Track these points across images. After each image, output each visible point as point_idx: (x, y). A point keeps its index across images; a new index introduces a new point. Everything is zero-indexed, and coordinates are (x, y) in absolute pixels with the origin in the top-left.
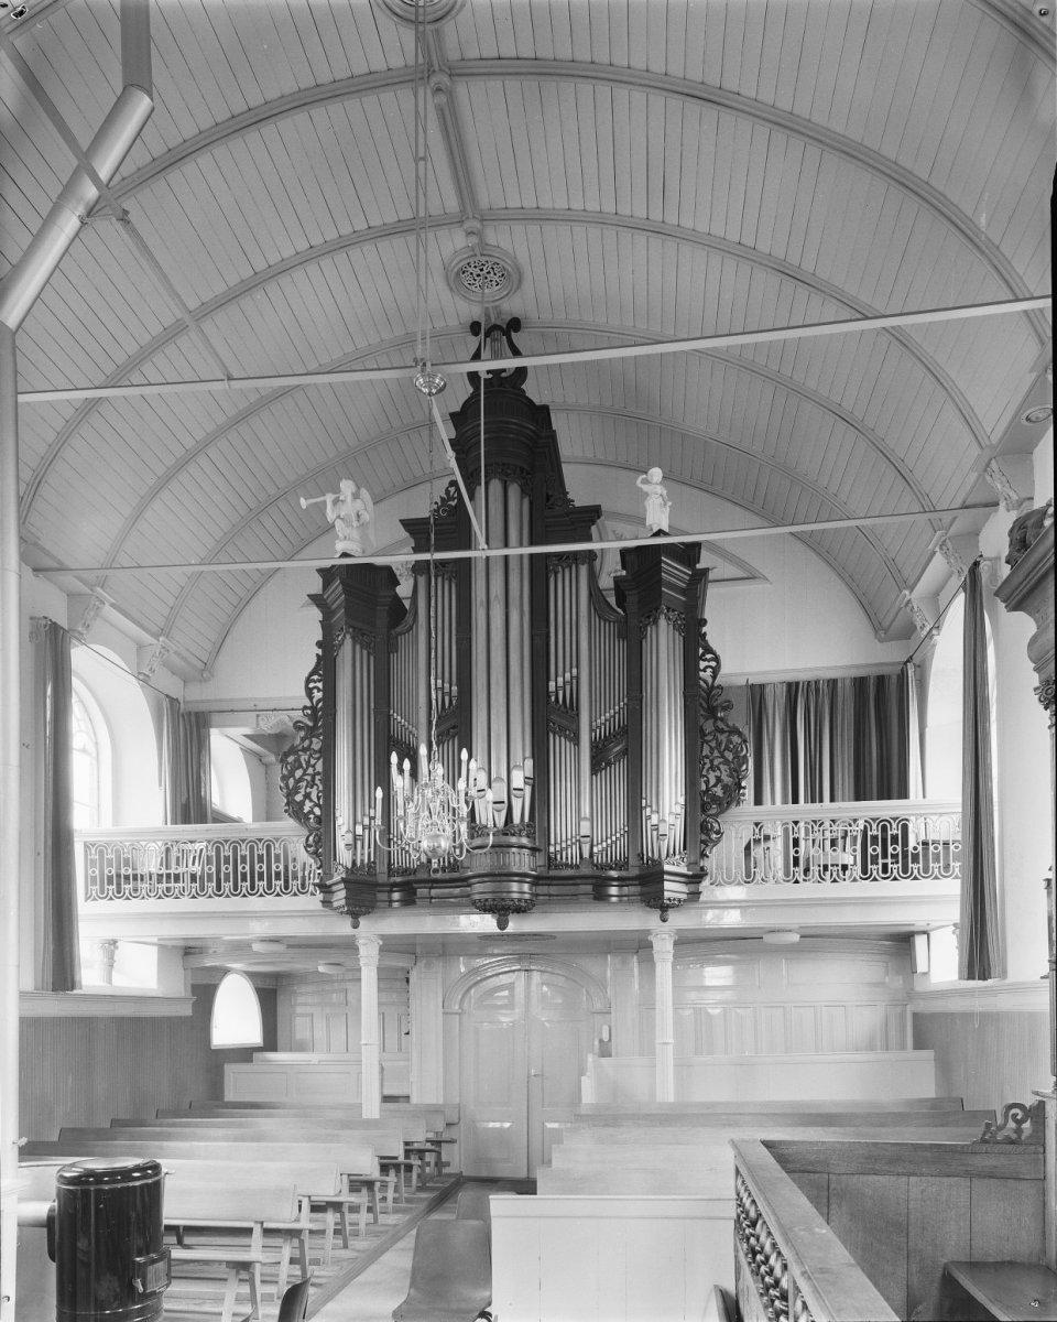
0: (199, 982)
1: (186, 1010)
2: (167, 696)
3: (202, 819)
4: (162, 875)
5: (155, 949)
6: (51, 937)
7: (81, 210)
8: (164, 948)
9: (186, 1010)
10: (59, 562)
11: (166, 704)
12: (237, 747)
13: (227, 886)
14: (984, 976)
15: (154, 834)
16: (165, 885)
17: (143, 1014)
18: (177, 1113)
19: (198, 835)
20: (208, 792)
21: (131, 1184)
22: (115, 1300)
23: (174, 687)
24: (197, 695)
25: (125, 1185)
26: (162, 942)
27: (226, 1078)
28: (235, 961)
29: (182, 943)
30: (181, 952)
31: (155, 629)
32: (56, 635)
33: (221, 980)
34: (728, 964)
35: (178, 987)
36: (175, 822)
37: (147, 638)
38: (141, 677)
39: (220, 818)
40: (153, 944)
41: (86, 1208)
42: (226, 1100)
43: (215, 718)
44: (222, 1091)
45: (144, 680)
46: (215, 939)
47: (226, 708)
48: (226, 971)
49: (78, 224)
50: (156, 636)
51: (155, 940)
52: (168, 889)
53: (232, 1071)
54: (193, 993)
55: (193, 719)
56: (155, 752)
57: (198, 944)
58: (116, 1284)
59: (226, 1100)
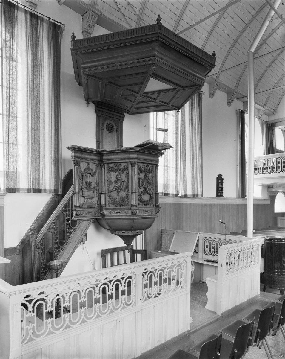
0: (272, 195)
1: (268, 202)
2: (265, 121)
3: (273, 152)
4: (265, 168)
5: (261, 186)
6: (240, 184)
7: (270, 19)
8: (263, 186)
9: (268, 202)
10: (243, 95)
11: (264, 123)
12: (281, 130)
13: (279, 170)
14: (134, 261)
15: (261, 157)
16: (266, 170)
17: (258, 203)
18: (267, 229)
19: (273, 158)
20: (275, 145)
21: (281, 242)
22: (279, 268)
23: (265, 118)
24: (271, 119)
25: (280, 242)
26: (263, 185)
27: (278, 220)
28: (281, 189)
29: (267, 185)
30: (267, 188)
31: (262, 105)
32: (242, 112)
33: (277, 194)
34: (174, 110)
35: (266, 197)
36: (267, 154)
37: (261, 108)
38: (259, 118)
39: (279, 151)
40: (260, 185)
41: (271, 248)
42: (278, 226)
43: (277, 124)
44: (277, 224)
45: (259, 118)
46: (276, 184)
47: (280, 121)
48: (278, 192)
49: (269, 22)
50: (263, 106)
51: (261, 185)
52: (267, 171)
53: (279, 219)
54: (270, 198)
55: (271, 125)
56: (261, 137)
57: (271, 185)
58: (279, 265)
59: (278, 226)
